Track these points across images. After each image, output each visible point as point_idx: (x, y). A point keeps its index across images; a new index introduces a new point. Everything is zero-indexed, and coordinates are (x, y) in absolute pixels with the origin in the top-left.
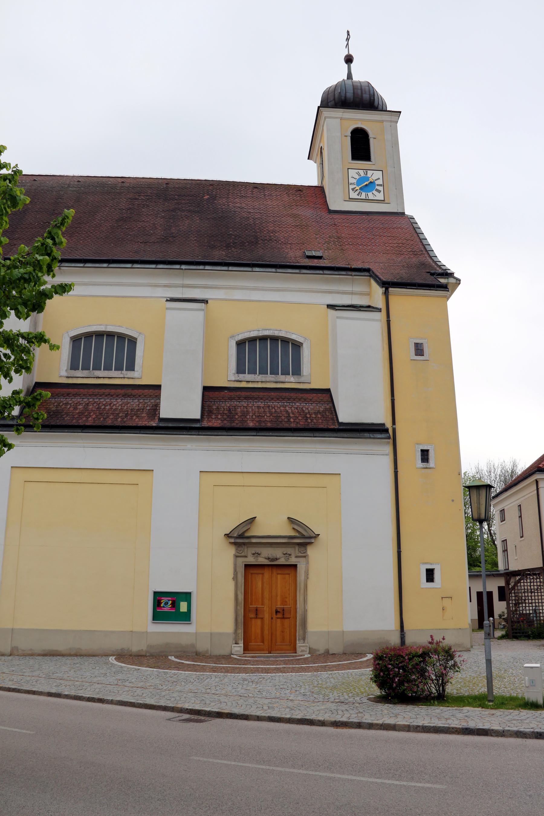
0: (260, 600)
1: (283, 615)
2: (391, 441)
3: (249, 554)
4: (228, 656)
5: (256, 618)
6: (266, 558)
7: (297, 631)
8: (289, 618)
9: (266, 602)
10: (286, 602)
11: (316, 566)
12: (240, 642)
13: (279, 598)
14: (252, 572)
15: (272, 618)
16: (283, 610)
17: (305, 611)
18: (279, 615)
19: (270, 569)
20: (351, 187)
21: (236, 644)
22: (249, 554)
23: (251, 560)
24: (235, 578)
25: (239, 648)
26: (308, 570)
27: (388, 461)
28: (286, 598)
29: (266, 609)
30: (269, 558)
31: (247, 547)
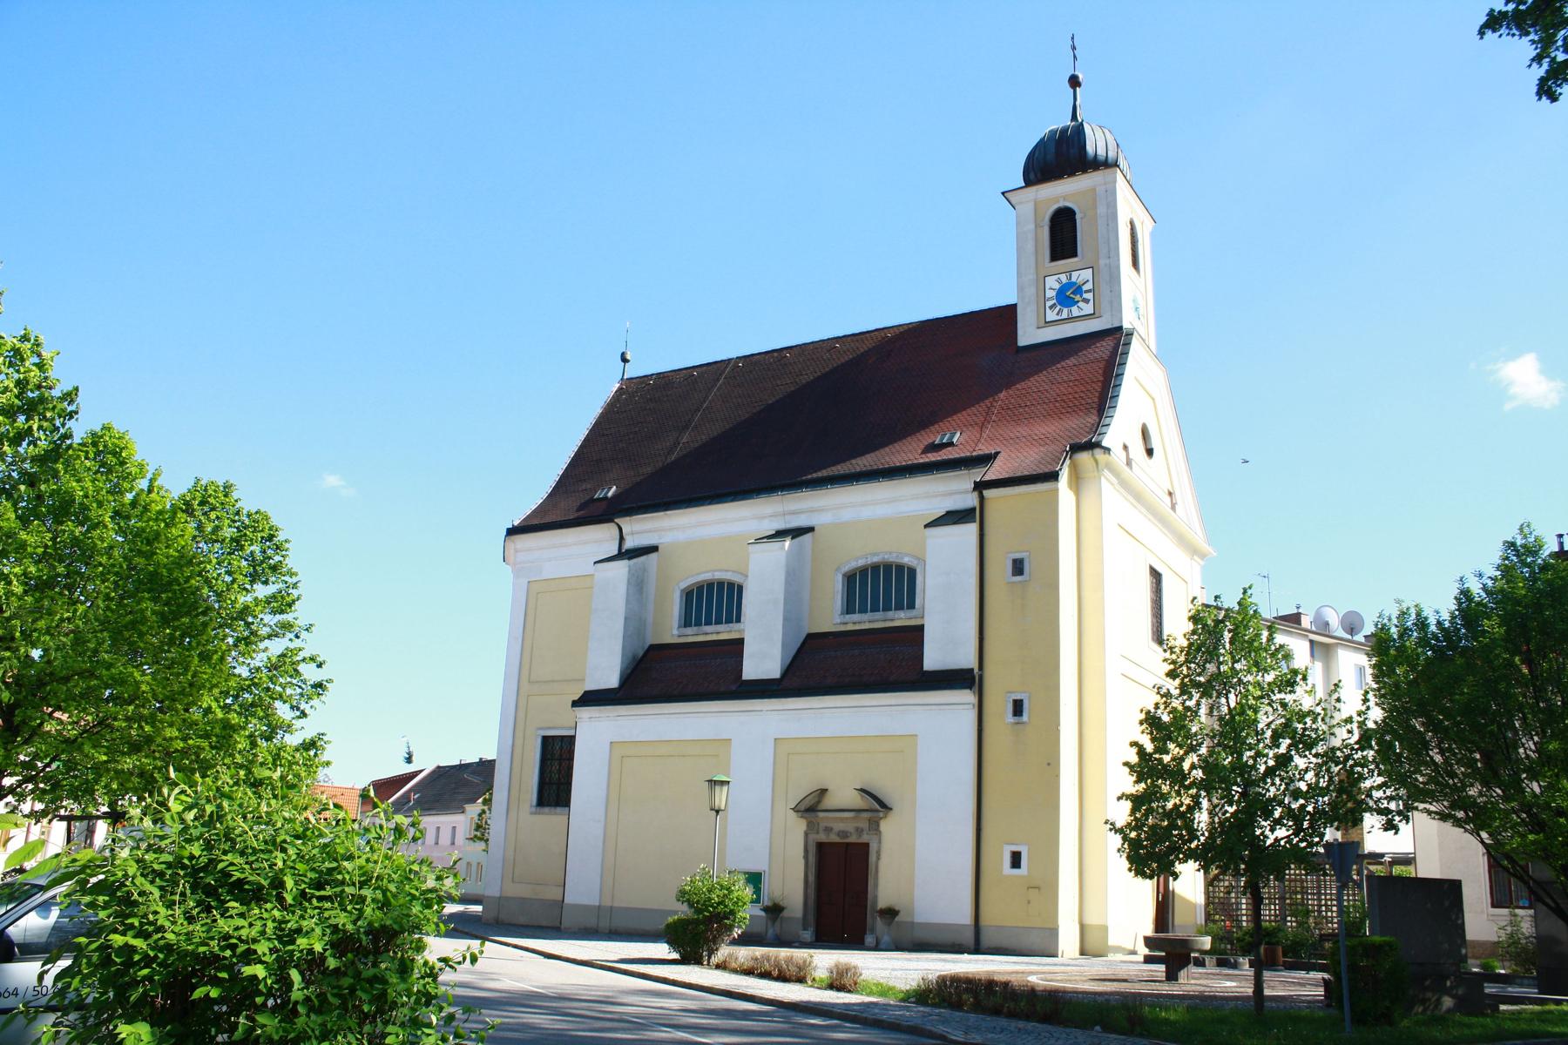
2: (976, 687)
11: (828, 795)
20: (1049, 304)
24: (806, 857)
27: (970, 716)
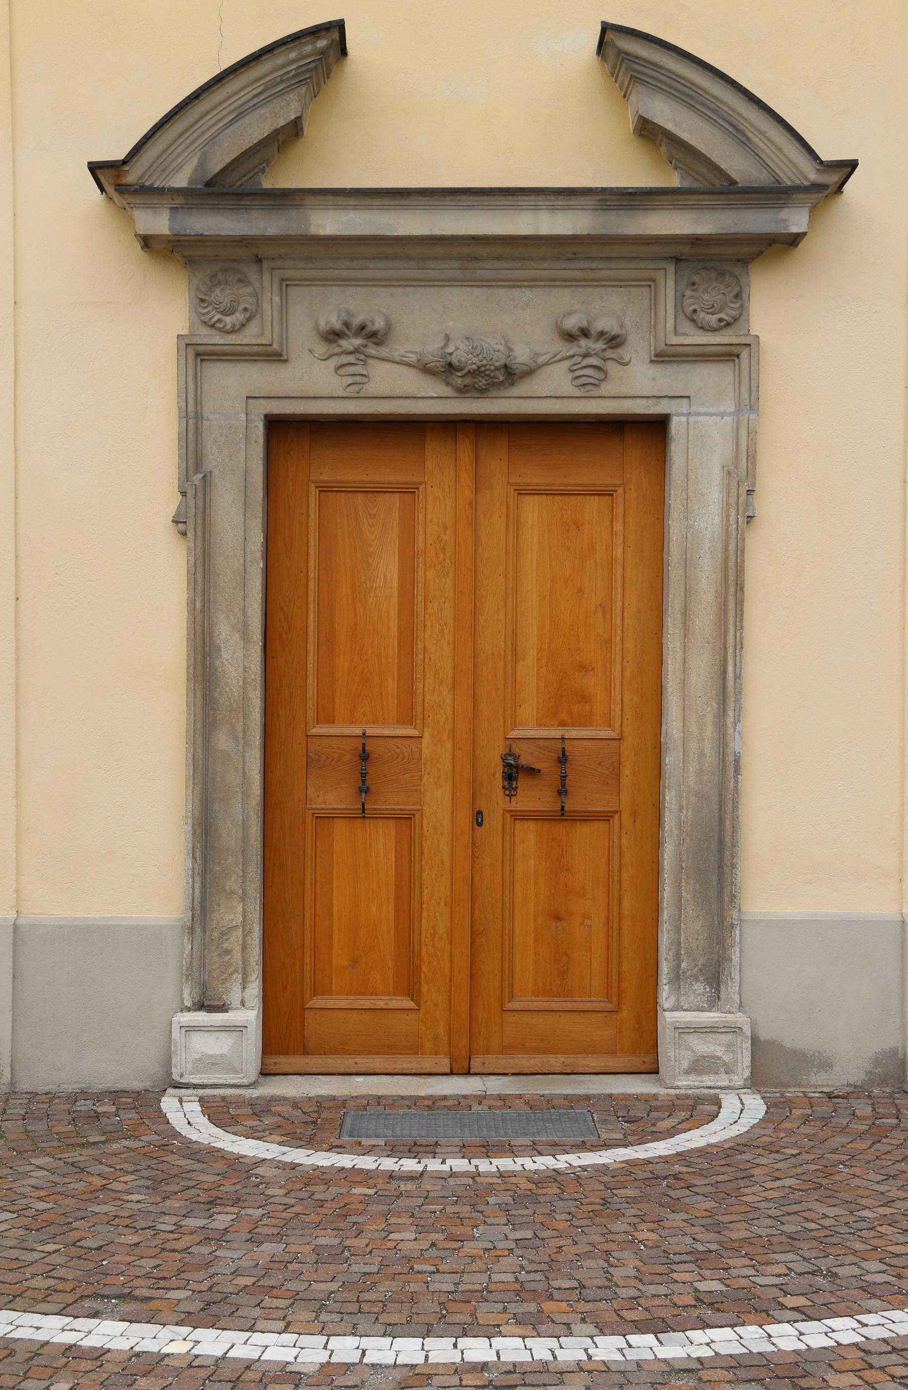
0: (392, 685)
1: (562, 792)
3: (302, 336)
4: (137, 1095)
5: (363, 813)
6: (426, 369)
7: (665, 916)
8: (606, 817)
9: (438, 696)
10: (584, 698)
12: (235, 995)
13: (529, 670)
14: (328, 475)
15: (478, 818)
16: (563, 759)
17: (727, 770)
18: (534, 797)
19: (465, 449)
21: (201, 1006)
22: (302, 336)
23: (314, 382)
24: (194, 519)
25: (226, 1042)
26: (752, 458)
28: (583, 668)
29: (436, 750)
30: (450, 367)
31: (286, 284)
